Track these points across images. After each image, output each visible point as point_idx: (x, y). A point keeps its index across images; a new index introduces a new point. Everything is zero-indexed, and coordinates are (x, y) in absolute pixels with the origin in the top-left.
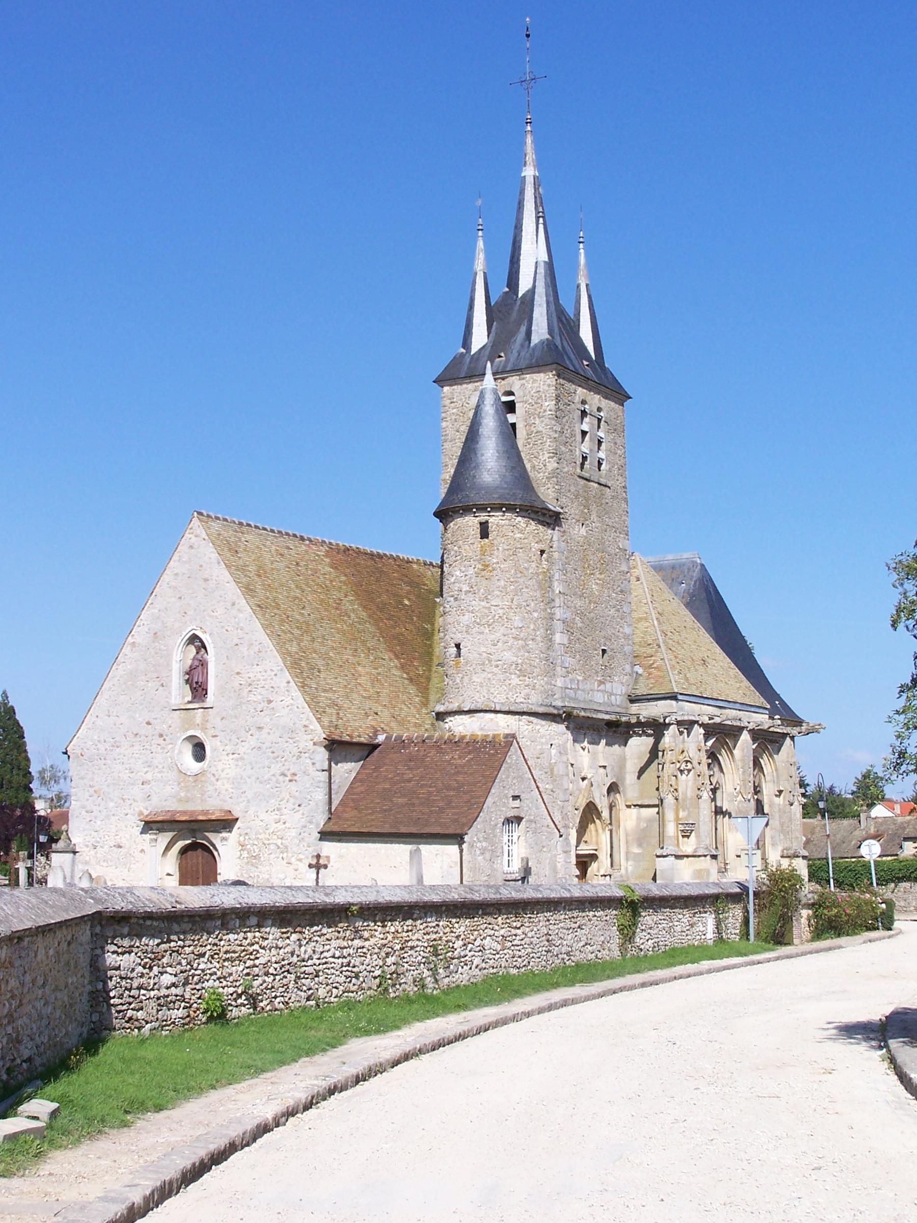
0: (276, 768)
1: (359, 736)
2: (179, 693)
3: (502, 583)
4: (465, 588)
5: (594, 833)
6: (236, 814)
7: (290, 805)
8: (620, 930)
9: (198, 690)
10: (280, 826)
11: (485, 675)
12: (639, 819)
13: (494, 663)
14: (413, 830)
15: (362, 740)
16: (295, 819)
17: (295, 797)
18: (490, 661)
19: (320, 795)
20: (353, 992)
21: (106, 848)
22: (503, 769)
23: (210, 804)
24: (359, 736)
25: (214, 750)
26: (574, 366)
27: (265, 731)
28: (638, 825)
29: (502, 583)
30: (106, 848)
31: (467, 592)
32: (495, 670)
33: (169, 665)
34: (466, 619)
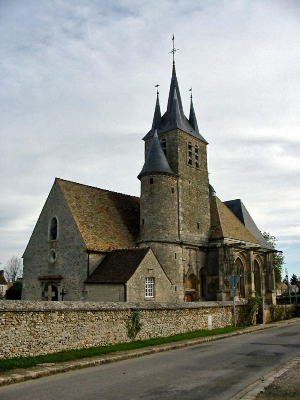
0: (73, 261)
1: (102, 249)
2: (48, 238)
3: (157, 198)
4: (145, 201)
5: (194, 267)
6: (63, 276)
7: (77, 274)
8: (192, 301)
9: (54, 235)
10: (74, 281)
11: (151, 230)
12: (212, 280)
13: (154, 225)
14: (111, 281)
15: (103, 251)
16: (78, 278)
17: (78, 271)
18: (153, 225)
19: (85, 270)
20: (178, 304)
21: (30, 288)
22: (155, 259)
23: (56, 274)
24: (102, 249)
25: (58, 255)
26: (184, 129)
27: (71, 248)
28: (212, 282)
29: (157, 198)
30: (30, 288)
31: (146, 202)
32: (154, 228)
33: (47, 228)
34: (145, 211)
